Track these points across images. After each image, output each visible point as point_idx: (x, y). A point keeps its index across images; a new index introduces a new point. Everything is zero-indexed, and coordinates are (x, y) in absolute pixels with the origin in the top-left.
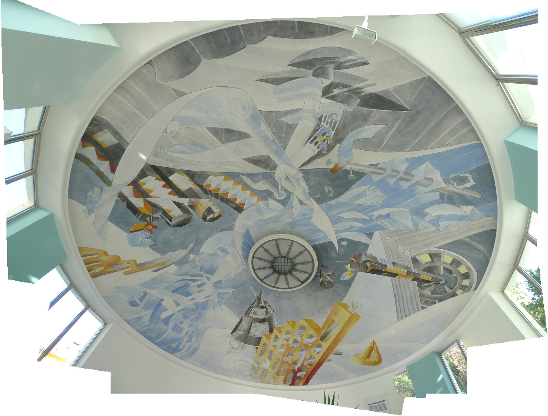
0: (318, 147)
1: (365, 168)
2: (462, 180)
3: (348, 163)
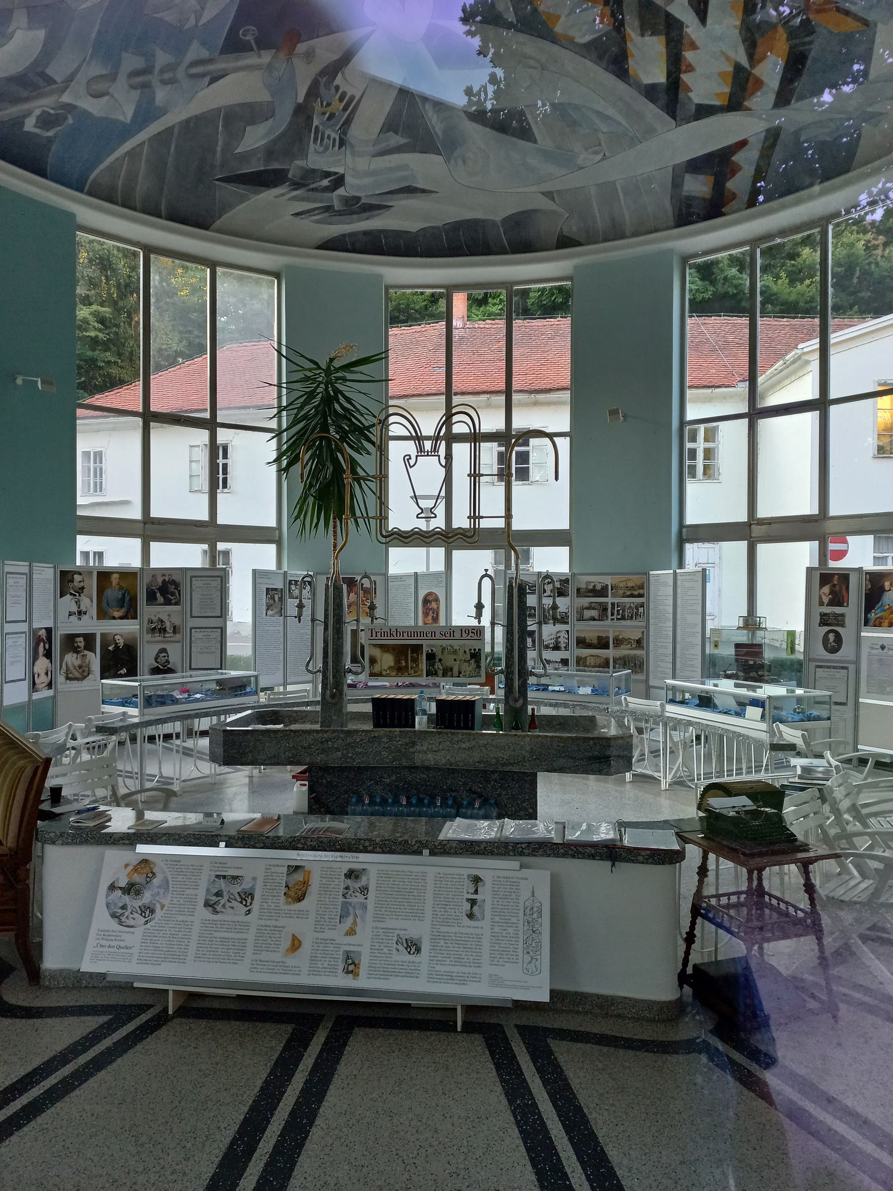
0: (337, 88)
1: (231, 65)
2: (46, 121)
3: (269, 67)
